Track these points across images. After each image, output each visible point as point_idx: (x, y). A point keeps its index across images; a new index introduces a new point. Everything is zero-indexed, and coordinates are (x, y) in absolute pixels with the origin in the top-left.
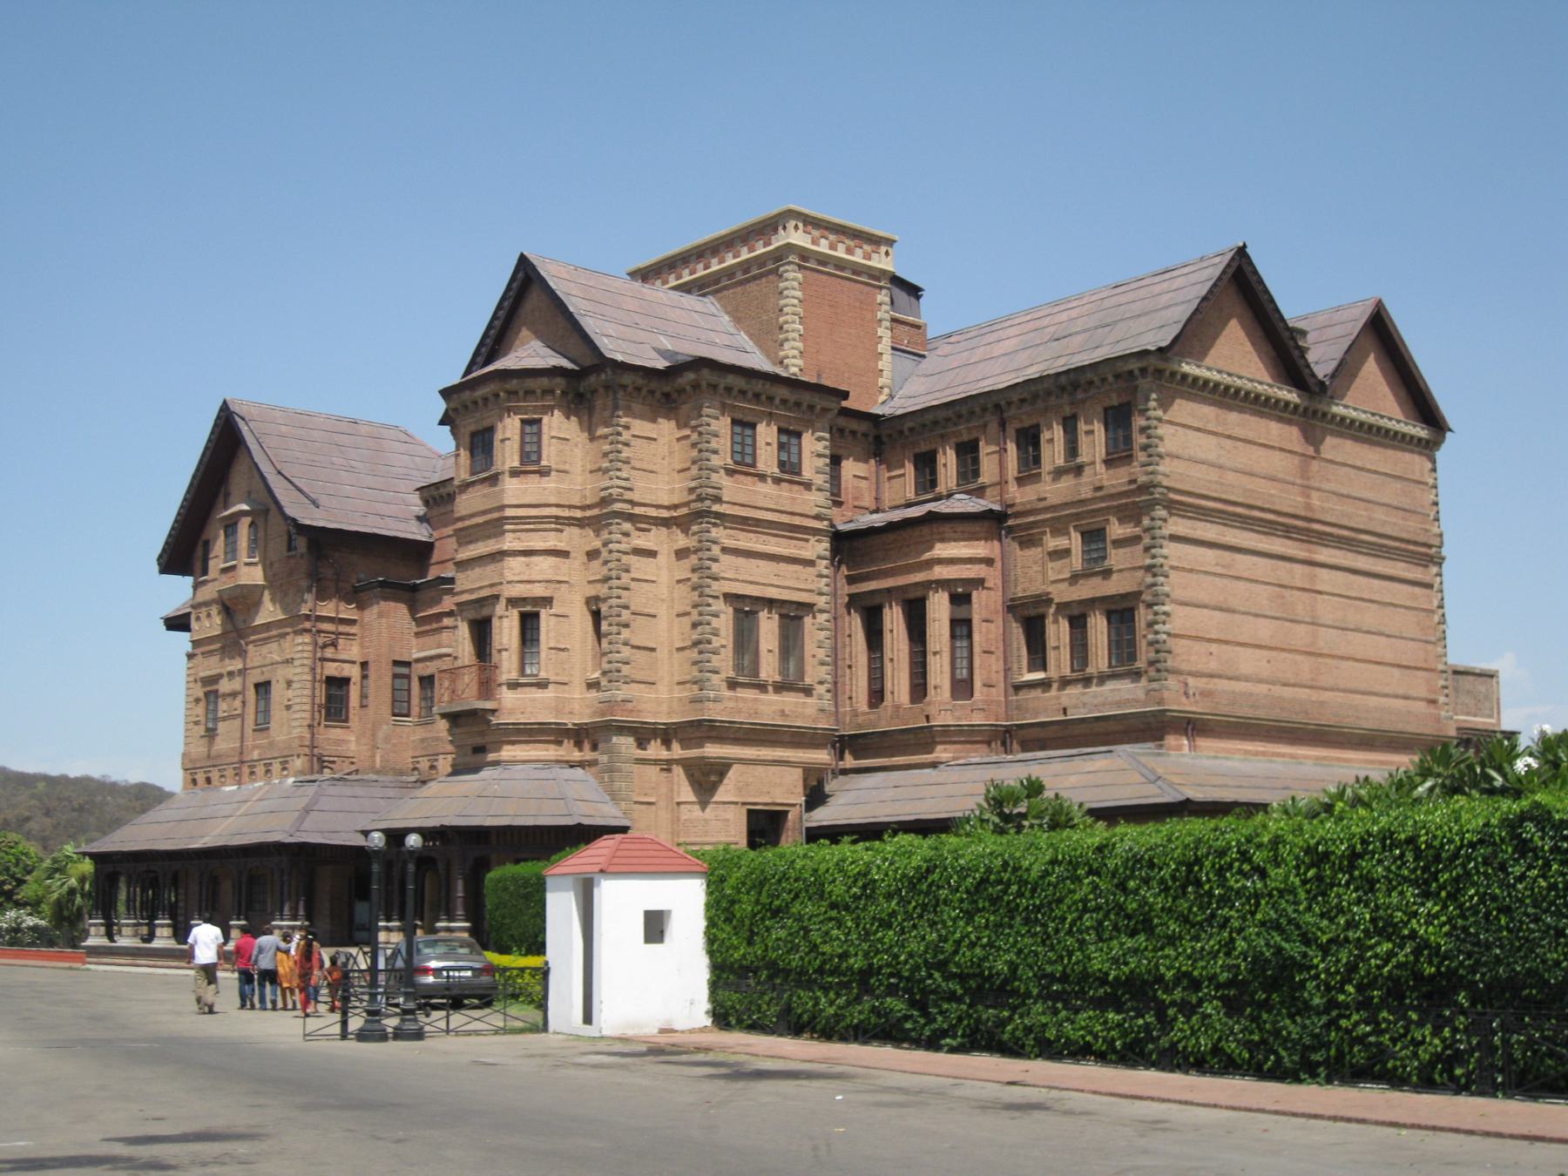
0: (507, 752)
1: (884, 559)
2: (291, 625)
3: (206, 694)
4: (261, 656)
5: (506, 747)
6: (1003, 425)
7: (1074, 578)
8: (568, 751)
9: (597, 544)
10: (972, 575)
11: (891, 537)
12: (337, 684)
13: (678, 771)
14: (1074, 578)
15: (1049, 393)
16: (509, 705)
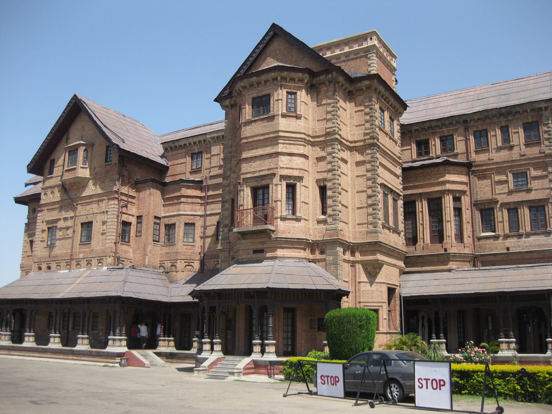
0: (280, 252)
1: (415, 181)
2: (107, 196)
3: (49, 228)
4: (84, 212)
5: (278, 250)
6: (467, 129)
7: (510, 193)
8: (306, 254)
9: (323, 154)
10: (462, 189)
11: (421, 171)
12: (126, 224)
13: (359, 267)
14: (510, 193)
15: (493, 117)
16: (282, 229)
